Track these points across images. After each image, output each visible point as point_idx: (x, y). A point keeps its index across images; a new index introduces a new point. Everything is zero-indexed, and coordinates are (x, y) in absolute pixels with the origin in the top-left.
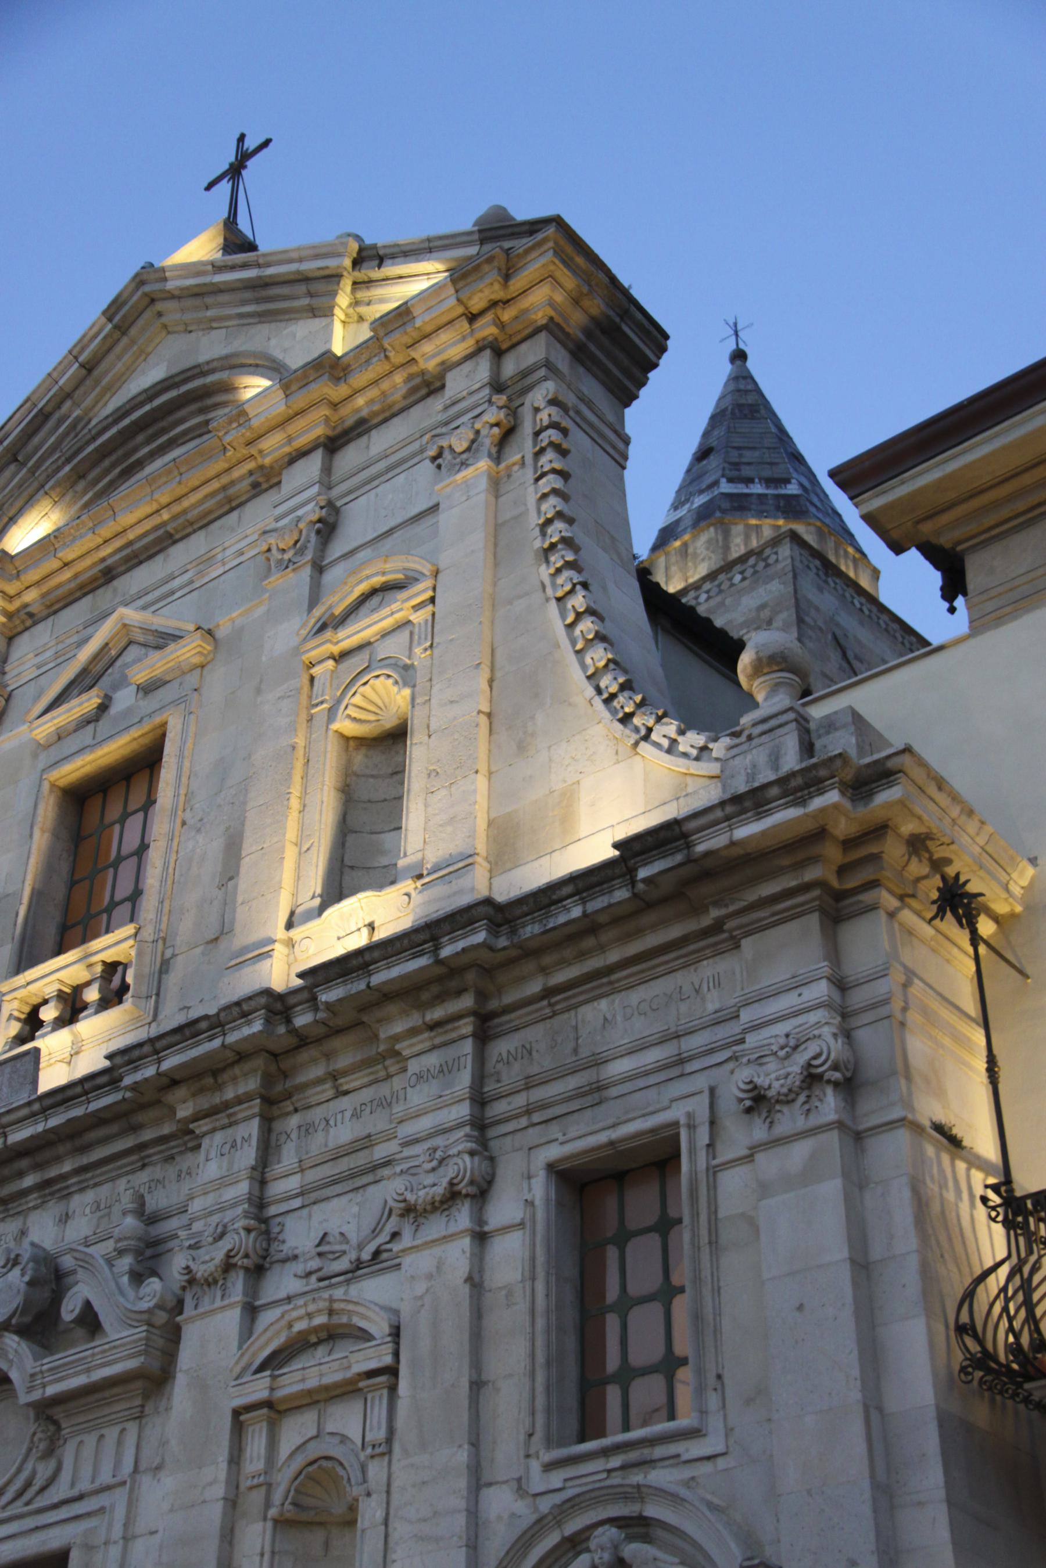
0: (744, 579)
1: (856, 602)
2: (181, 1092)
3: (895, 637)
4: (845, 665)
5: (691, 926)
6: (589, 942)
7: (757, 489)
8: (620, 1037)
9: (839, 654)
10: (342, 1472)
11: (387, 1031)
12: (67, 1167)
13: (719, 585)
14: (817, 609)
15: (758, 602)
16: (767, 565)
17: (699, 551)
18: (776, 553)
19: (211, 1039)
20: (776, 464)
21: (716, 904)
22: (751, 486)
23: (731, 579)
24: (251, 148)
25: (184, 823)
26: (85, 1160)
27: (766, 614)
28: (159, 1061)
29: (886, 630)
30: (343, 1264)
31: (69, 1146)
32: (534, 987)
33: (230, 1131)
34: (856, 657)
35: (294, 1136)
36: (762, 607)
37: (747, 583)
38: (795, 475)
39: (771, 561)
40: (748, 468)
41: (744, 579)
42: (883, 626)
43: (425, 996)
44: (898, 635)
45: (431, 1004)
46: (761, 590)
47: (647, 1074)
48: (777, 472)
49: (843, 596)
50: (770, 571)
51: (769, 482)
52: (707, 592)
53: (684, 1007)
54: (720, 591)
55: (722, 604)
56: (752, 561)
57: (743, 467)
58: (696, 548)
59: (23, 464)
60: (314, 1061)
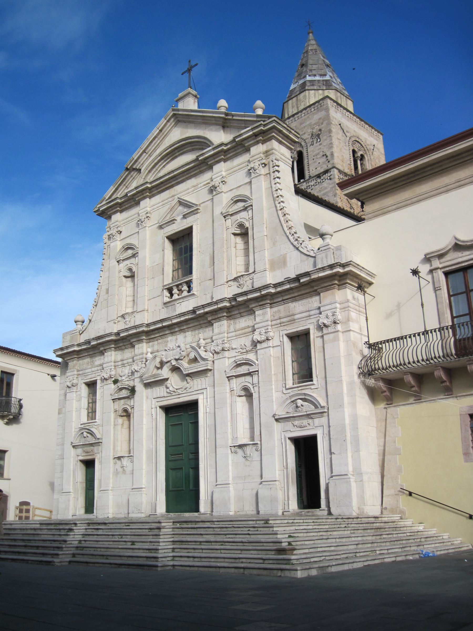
0: (314, 110)
1: (346, 114)
2: (209, 315)
3: (358, 123)
4: (344, 135)
5: (311, 290)
6: (291, 292)
7: (317, 78)
8: (297, 311)
9: (342, 131)
10: (246, 387)
11: (251, 306)
12: (185, 327)
13: (308, 112)
14: (336, 119)
15: (319, 117)
16: (321, 106)
17: (301, 99)
18: (323, 102)
19: (215, 306)
20: (323, 69)
21: (316, 286)
22: (315, 77)
23: (311, 110)
24: (193, 65)
25: (199, 252)
26: (189, 326)
27: (321, 121)
28: (204, 309)
29: (355, 121)
30: (245, 351)
31: (185, 323)
32: (280, 299)
33: (219, 322)
34: (347, 132)
35: (232, 324)
36: (320, 119)
37: (315, 111)
38: (328, 73)
39: (322, 105)
40: (314, 71)
41: (314, 110)
42: (354, 120)
43: (258, 300)
44: (359, 122)
45: (260, 302)
46: (319, 114)
47: (303, 318)
48: (322, 72)
49: (343, 113)
50: (322, 108)
51: (321, 75)
52: (304, 113)
53: (310, 305)
54: (308, 113)
55: (308, 117)
56: (317, 104)
57: (313, 71)
58: (300, 99)
59: (147, 153)
60: (236, 310)
